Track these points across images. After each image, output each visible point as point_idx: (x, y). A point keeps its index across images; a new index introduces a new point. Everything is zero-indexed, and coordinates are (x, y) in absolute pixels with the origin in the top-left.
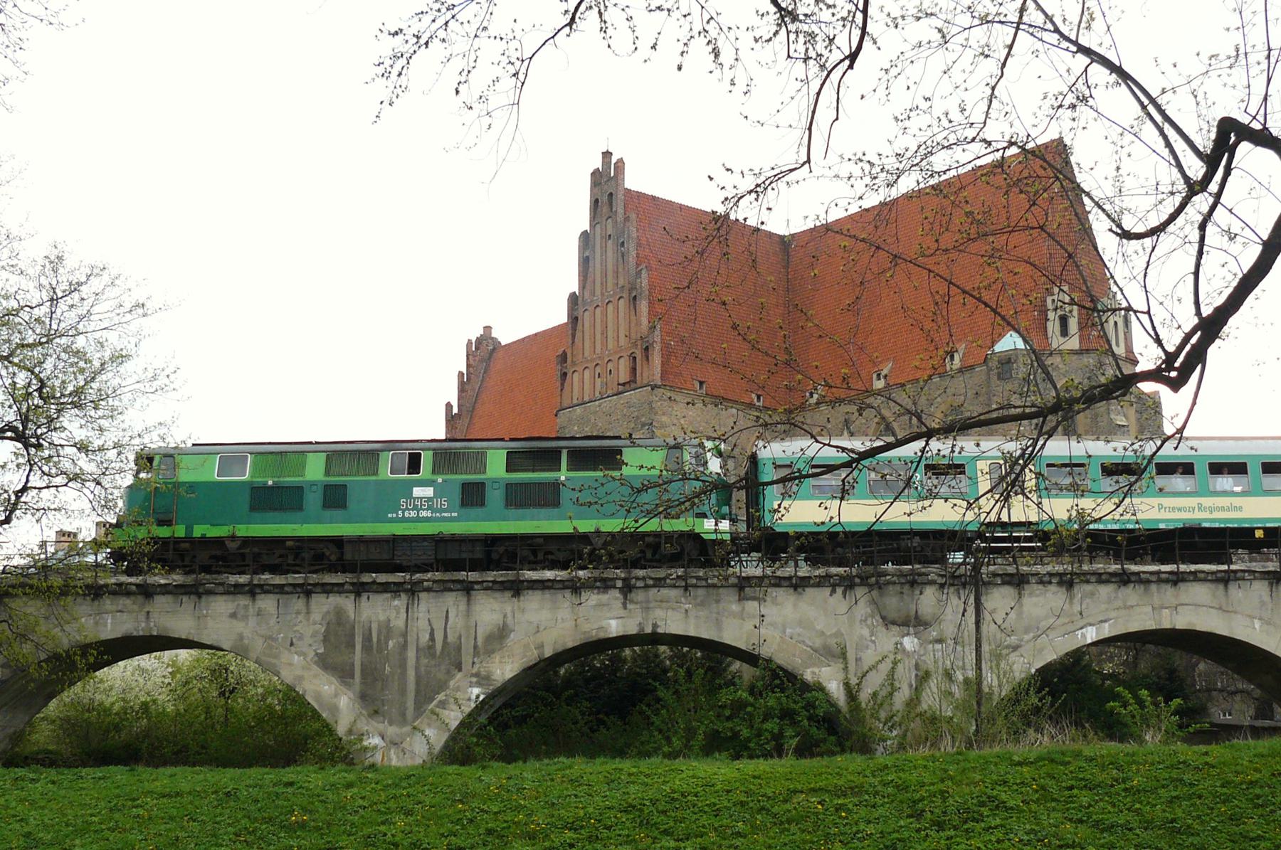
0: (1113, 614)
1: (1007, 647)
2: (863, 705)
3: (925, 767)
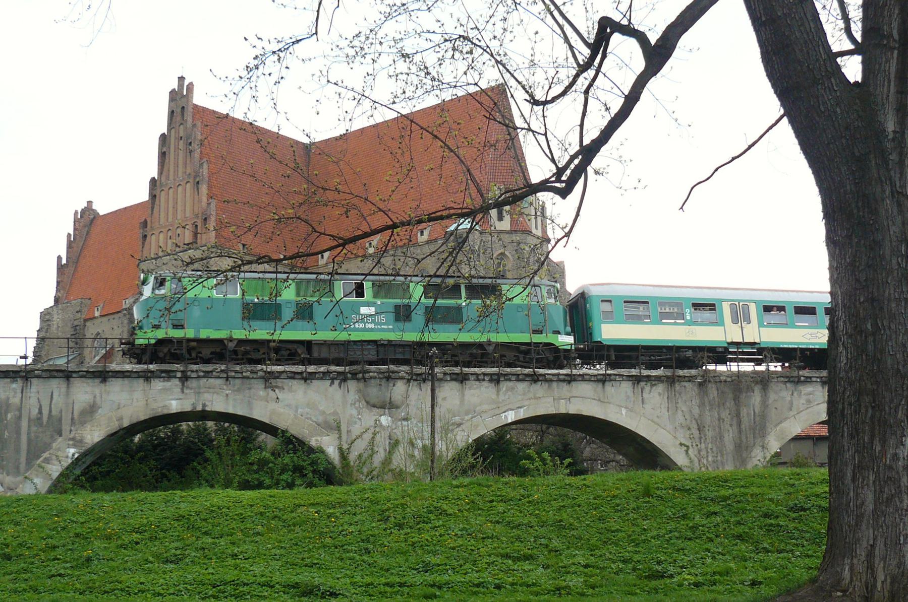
0: (526, 403)
1: (453, 424)
2: (352, 463)
3: (392, 489)
